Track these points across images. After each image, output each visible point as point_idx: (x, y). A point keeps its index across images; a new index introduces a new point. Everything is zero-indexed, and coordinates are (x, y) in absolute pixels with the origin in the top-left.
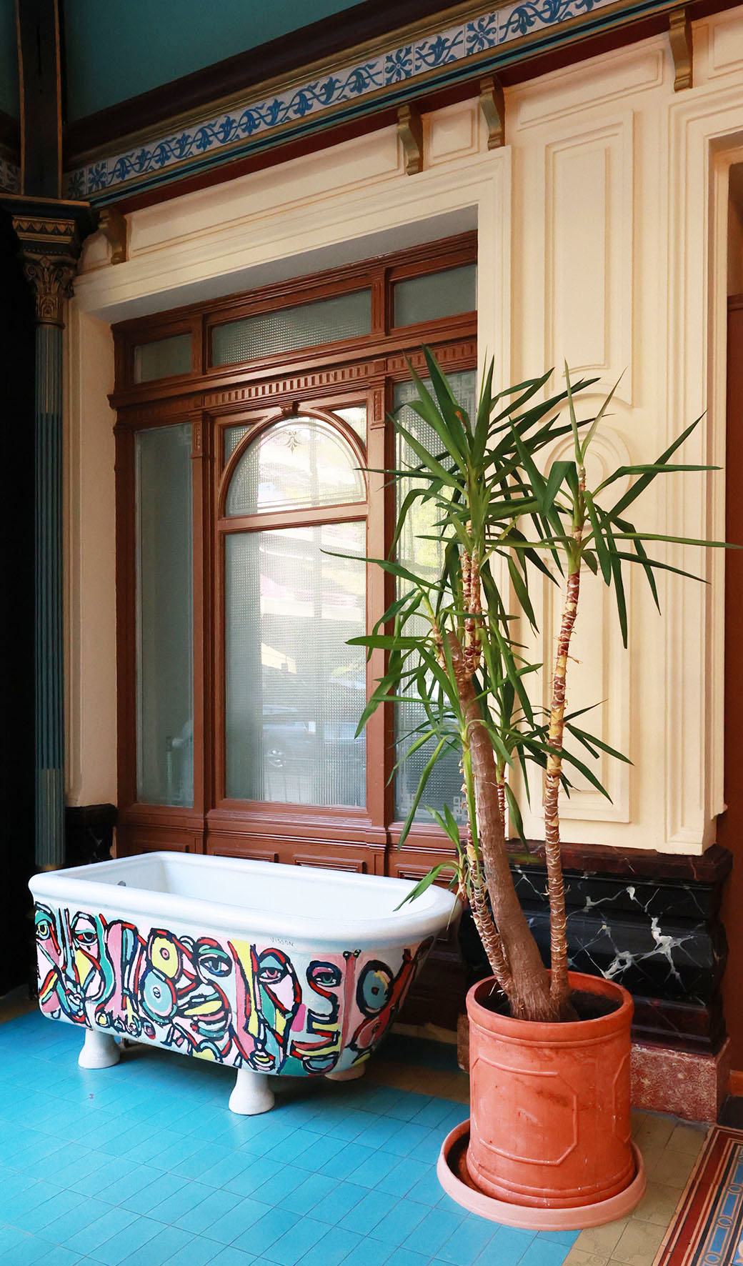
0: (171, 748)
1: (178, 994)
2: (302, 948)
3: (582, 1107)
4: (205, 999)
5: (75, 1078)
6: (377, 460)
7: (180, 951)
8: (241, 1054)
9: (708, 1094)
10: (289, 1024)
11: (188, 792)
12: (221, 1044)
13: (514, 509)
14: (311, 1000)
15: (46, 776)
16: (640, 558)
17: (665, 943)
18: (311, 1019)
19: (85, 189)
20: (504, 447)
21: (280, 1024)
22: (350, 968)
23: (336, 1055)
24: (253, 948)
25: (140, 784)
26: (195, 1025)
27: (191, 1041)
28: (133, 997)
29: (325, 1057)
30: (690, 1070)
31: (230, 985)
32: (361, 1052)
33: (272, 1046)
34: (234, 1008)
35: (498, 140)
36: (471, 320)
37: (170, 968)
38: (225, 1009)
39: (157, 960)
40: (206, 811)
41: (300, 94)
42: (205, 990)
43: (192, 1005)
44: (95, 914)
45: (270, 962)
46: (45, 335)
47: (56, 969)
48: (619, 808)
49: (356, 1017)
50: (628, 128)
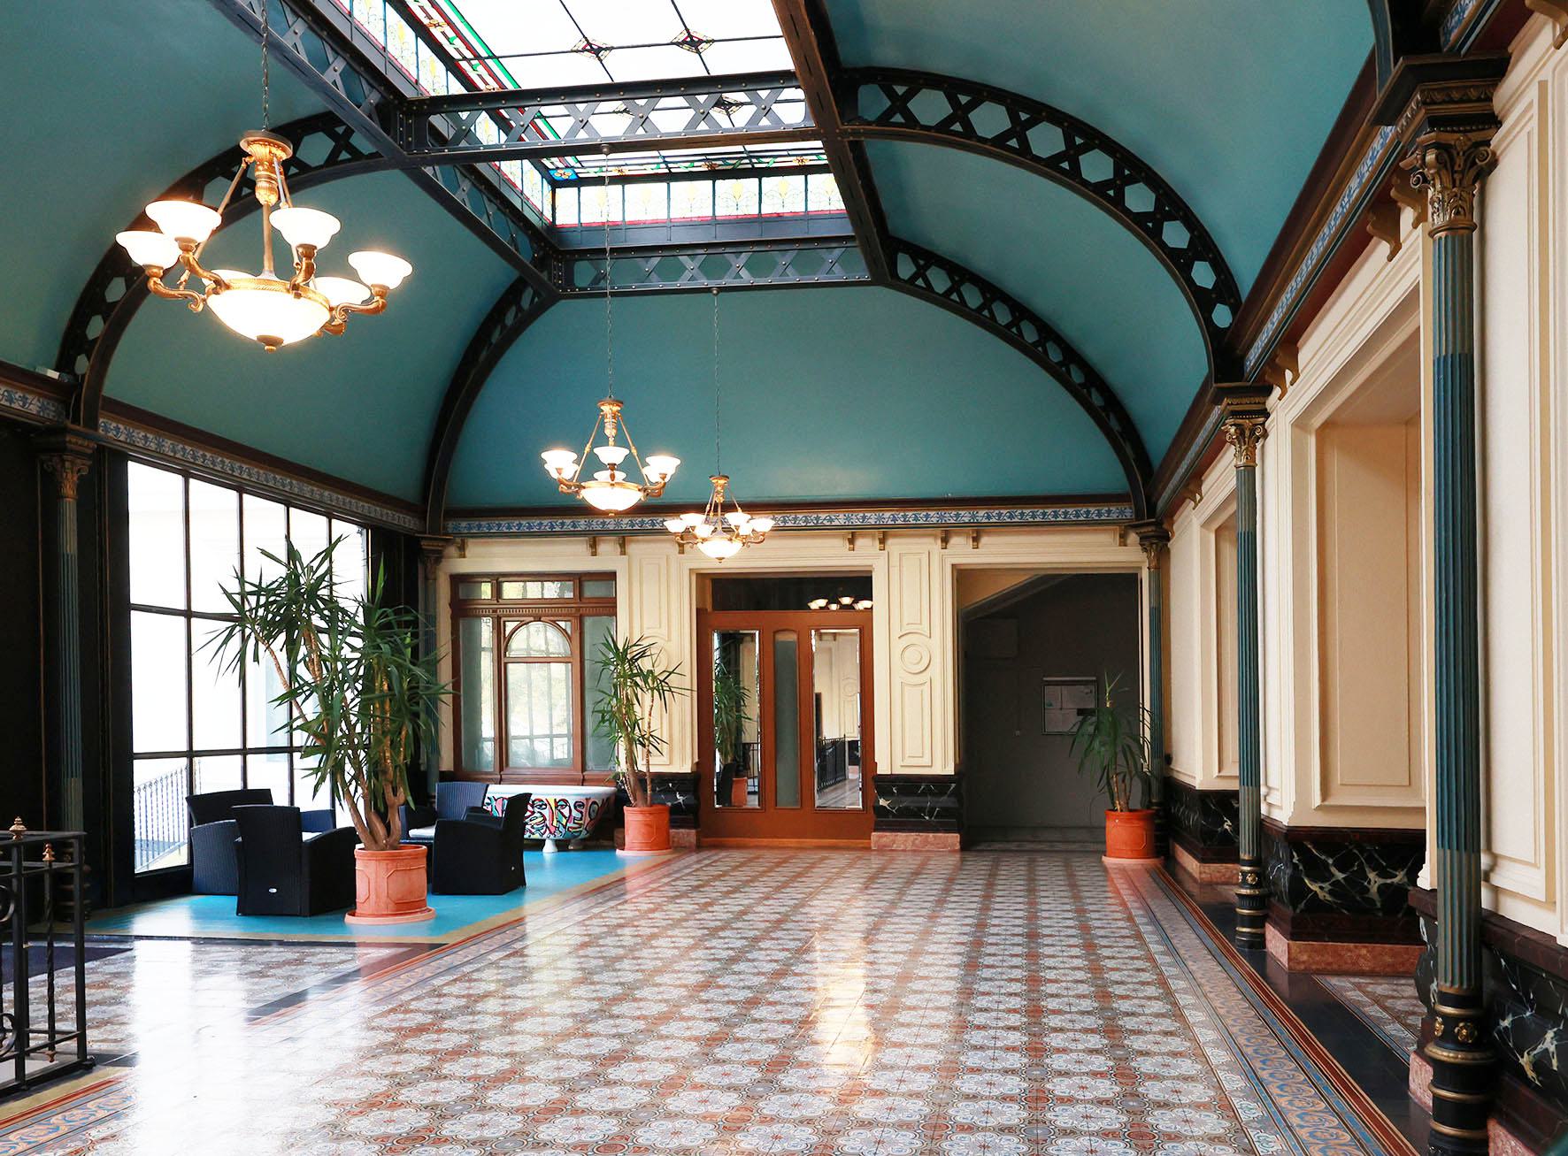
6: (791, 853)
14: (575, 813)
16: (670, 690)
17: (680, 798)
21: (564, 821)
26: (532, 827)
30: (688, 834)
31: (546, 812)
33: (561, 829)
36: (614, 600)
38: (545, 819)
45: (562, 803)
48: (665, 759)
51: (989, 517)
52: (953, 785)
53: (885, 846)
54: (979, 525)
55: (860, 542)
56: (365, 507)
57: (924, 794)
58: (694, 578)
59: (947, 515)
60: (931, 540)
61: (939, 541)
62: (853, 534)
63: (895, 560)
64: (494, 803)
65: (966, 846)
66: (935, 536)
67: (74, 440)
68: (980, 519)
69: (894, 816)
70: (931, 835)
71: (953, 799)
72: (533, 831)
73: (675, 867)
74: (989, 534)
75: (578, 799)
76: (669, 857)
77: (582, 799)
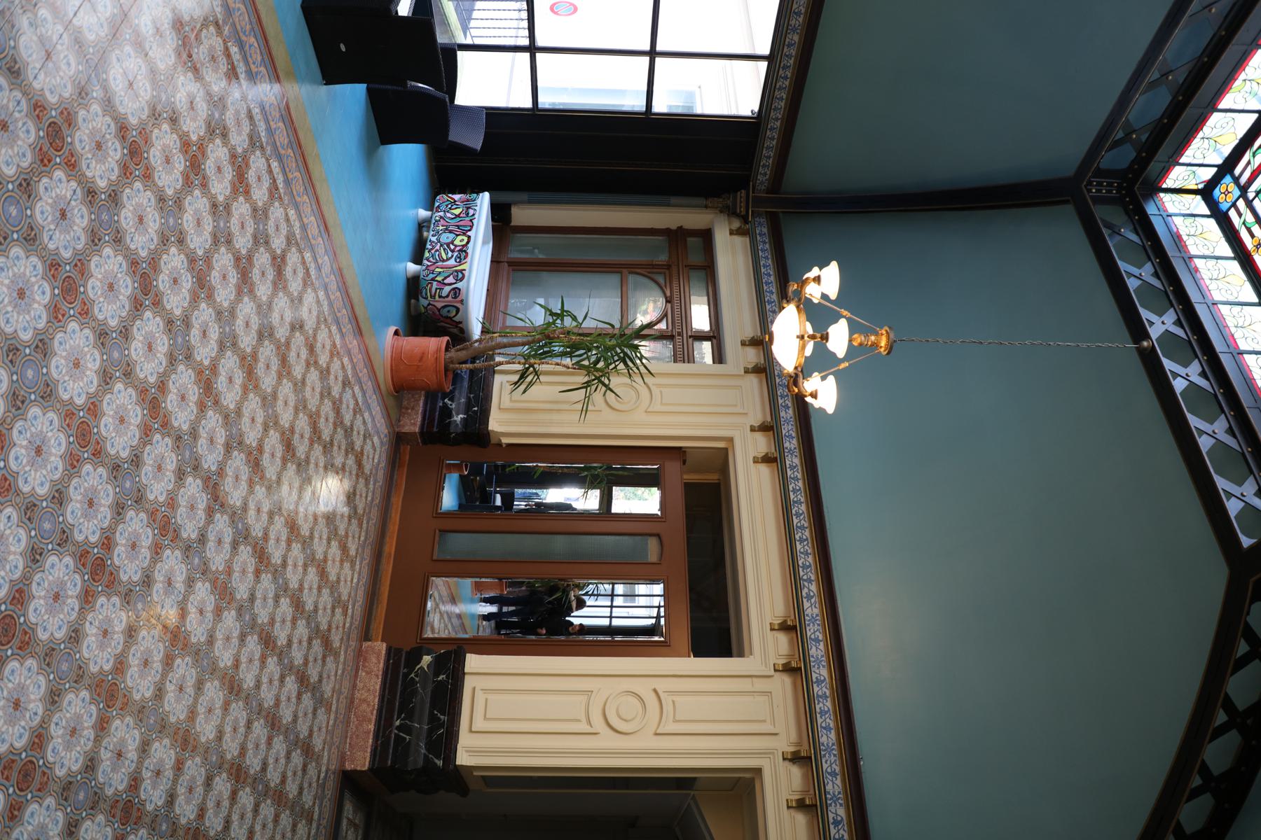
0: (534, 249)
1: (448, 245)
2: (465, 286)
3: (418, 366)
4: (447, 254)
5: (416, 207)
7: (463, 246)
8: (428, 266)
9: (406, 429)
10: (440, 282)
11: (514, 255)
12: (431, 259)
13: (605, 360)
14: (447, 289)
15: (524, 196)
17: (458, 418)
18: (440, 289)
19: (757, 219)
20: (626, 354)
21: (439, 278)
22: (458, 302)
23: (426, 298)
24: (465, 270)
25: (519, 235)
26: (437, 251)
27: (432, 249)
28: (446, 229)
29: (426, 294)
30: (415, 424)
31: (452, 262)
32: (426, 308)
33: (431, 276)
34: (445, 263)
35: (747, 371)
37: (457, 242)
38: (444, 261)
39: (460, 238)
40: (507, 262)
41: (774, 301)
42: (450, 254)
43: (444, 249)
44: (476, 216)
45: (460, 275)
46: (702, 201)
47: (455, 201)
48: (506, 403)
49: (439, 305)
50: (742, 411)
51: (836, 823)
52: (440, 763)
53: (365, 660)
54: (825, 807)
55: (783, 638)
56: (777, 117)
57: (433, 719)
58: (721, 445)
59: (833, 759)
60: (793, 736)
61: (792, 749)
62: (794, 628)
63: (760, 685)
64: (468, 219)
65: (349, 781)
66: (799, 744)
67: (743, 195)
68: (832, 809)
69: (406, 675)
70: (372, 727)
71: (421, 763)
72: (433, 251)
73: (369, 386)
74: (810, 825)
75: (463, 292)
76: (382, 386)
77: (462, 296)
